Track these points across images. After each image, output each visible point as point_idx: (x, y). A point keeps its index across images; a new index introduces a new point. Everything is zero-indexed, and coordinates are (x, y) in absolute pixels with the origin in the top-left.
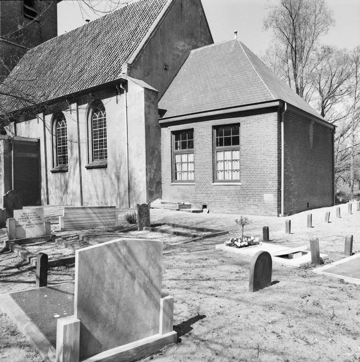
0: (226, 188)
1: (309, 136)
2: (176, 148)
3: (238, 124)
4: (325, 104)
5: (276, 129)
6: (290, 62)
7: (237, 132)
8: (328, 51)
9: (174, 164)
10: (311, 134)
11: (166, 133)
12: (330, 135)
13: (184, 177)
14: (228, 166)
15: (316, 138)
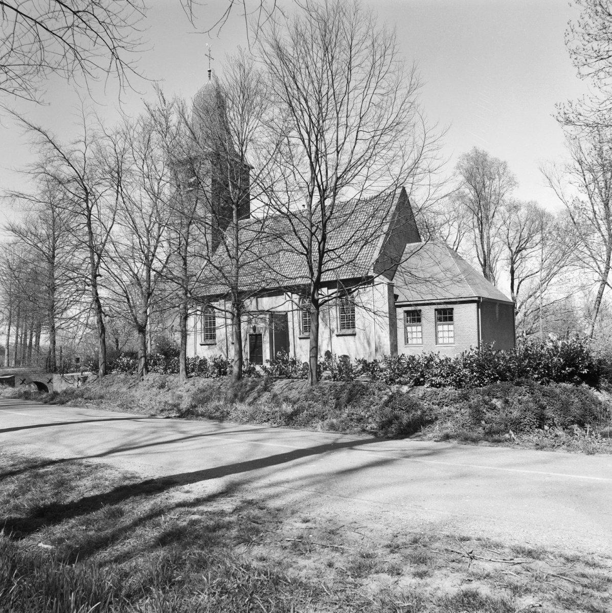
0: (445, 348)
2: (407, 322)
3: (453, 309)
4: (515, 259)
5: (476, 312)
6: (477, 231)
7: (451, 313)
8: (515, 208)
9: (406, 332)
10: (497, 311)
11: (400, 312)
13: (414, 341)
14: (446, 334)
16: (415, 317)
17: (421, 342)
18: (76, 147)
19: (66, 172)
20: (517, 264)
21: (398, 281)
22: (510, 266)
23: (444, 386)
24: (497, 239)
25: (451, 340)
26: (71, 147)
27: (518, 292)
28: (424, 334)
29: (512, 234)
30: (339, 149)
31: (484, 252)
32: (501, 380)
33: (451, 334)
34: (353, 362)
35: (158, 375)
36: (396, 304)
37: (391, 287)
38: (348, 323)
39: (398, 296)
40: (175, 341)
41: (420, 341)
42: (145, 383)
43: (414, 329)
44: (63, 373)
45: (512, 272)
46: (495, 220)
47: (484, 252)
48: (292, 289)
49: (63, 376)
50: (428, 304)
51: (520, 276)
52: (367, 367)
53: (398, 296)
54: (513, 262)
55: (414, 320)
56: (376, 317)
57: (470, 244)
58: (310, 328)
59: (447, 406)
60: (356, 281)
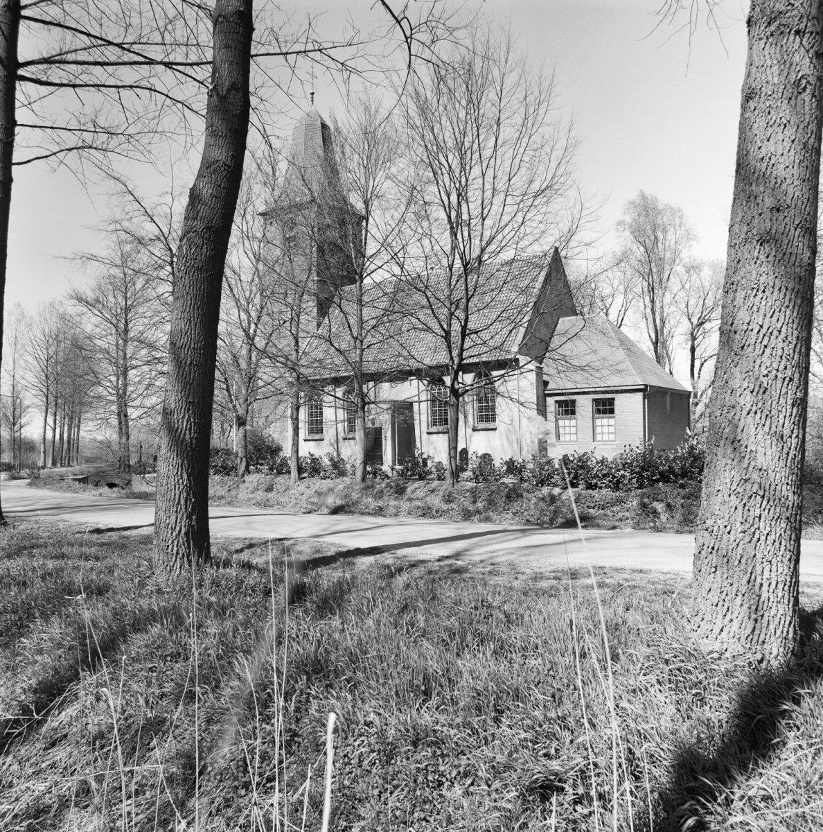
0: (604, 447)
1: (666, 405)
3: (614, 399)
8: (692, 269)
10: (668, 402)
11: (551, 401)
12: (686, 400)
13: (567, 438)
14: (606, 430)
15: (672, 405)
16: (568, 408)
17: (575, 439)
18: (162, 200)
19: (149, 230)
20: (699, 340)
21: (549, 367)
22: (690, 343)
23: (601, 488)
24: (673, 308)
25: (612, 437)
26: (156, 200)
27: (699, 377)
28: (579, 430)
29: (692, 302)
30: (485, 212)
31: (656, 326)
32: (663, 482)
33: (612, 429)
34: (497, 463)
35: (263, 476)
36: (546, 392)
37: (539, 372)
38: (487, 415)
39: (548, 382)
40: (270, 435)
41: (574, 438)
42: (246, 485)
43: (567, 422)
44: (144, 473)
45: (693, 350)
46: (670, 284)
47: (656, 326)
48: (418, 374)
49: (144, 477)
50: (584, 393)
51: (703, 355)
52: (512, 467)
53: (548, 382)
54: (694, 339)
55: (567, 413)
56: (522, 409)
57: (639, 316)
58: (445, 420)
59: (603, 509)
60: (501, 365)
